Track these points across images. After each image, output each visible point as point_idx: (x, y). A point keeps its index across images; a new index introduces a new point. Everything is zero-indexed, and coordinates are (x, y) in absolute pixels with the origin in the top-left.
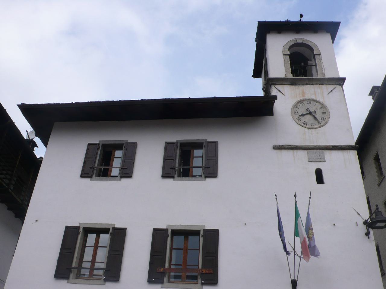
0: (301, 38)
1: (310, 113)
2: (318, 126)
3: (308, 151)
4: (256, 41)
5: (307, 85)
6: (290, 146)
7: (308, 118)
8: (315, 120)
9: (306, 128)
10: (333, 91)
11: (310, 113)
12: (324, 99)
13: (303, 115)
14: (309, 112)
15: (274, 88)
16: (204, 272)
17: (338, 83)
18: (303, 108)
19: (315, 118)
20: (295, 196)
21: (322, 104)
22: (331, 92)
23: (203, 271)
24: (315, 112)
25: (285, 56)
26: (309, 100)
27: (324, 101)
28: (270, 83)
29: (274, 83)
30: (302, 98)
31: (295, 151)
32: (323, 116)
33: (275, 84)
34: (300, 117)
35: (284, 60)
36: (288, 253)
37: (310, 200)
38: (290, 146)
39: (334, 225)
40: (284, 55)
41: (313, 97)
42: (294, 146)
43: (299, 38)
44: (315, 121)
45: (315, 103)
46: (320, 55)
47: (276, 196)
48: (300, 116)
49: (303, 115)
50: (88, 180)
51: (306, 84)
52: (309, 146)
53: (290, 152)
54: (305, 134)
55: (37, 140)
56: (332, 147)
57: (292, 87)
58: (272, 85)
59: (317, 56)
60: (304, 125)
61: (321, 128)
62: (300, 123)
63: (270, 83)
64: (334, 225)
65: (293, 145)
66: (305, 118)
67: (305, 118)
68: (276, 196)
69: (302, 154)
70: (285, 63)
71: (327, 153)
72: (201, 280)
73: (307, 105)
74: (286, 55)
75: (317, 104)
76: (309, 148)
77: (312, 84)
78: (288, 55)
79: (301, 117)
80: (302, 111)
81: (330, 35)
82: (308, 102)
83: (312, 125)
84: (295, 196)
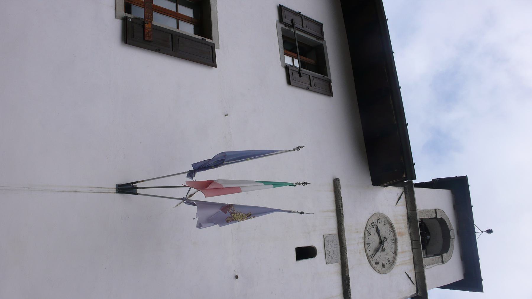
0: (454, 237)
1: (381, 243)
2: (369, 255)
3: (337, 236)
4: (433, 180)
5: (410, 241)
6: (342, 206)
7: (374, 240)
8: (375, 251)
9: (364, 234)
10: (409, 280)
11: (381, 243)
12: (399, 265)
13: (378, 231)
14: (382, 240)
15: (402, 191)
16: (146, 25)
17: (419, 289)
18: (386, 232)
19: (377, 250)
20: (304, 184)
21: (394, 263)
22: (407, 277)
23: (148, 23)
24: (383, 250)
25: (434, 211)
26: (395, 242)
27: (397, 265)
28: (406, 186)
29: (407, 192)
30: (397, 231)
31: (334, 214)
32: (380, 263)
33: (405, 192)
34: (375, 227)
35: (431, 210)
36: (191, 174)
37: (297, 212)
38: (341, 205)
39: (237, 277)
40: (435, 210)
41: (400, 249)
42: (342, 212)
43: (454, 233)
44: (374, 249)
45: (393, 251)
46: (443, 262)
47: (299, 148)
48: (377, 226)
49: (378, 231)
50: (219, 53)
51: (411, 239)
52: (345, 236)
53: (331, 205)
54: (357, 232)
55: (190, 180)
56: (347, 275)
57: (406, 218)
58: (404, 189)
59: (441, 258)
60: (367, 233)
61: (366, 257)
62: (368, 227)
63: (406, 186)
64: (237, 277)
65: (343, 209)
66: (375, 234)
67: (375, 234)
68: (299, 148)
69: (332, 227)
70: (428, 210)
71: (336, 268)
72: (132, 18)
73: (390, 237)
74: (436, 213)
75: (392, 255)
76: (342, 236)
77: (412, 249)
78: (436, 216)
79: (375, 229)
80: (384, 231)
81: (462, 279)
82: (392, 240)
83: (369, 244)
84: (304, 184)
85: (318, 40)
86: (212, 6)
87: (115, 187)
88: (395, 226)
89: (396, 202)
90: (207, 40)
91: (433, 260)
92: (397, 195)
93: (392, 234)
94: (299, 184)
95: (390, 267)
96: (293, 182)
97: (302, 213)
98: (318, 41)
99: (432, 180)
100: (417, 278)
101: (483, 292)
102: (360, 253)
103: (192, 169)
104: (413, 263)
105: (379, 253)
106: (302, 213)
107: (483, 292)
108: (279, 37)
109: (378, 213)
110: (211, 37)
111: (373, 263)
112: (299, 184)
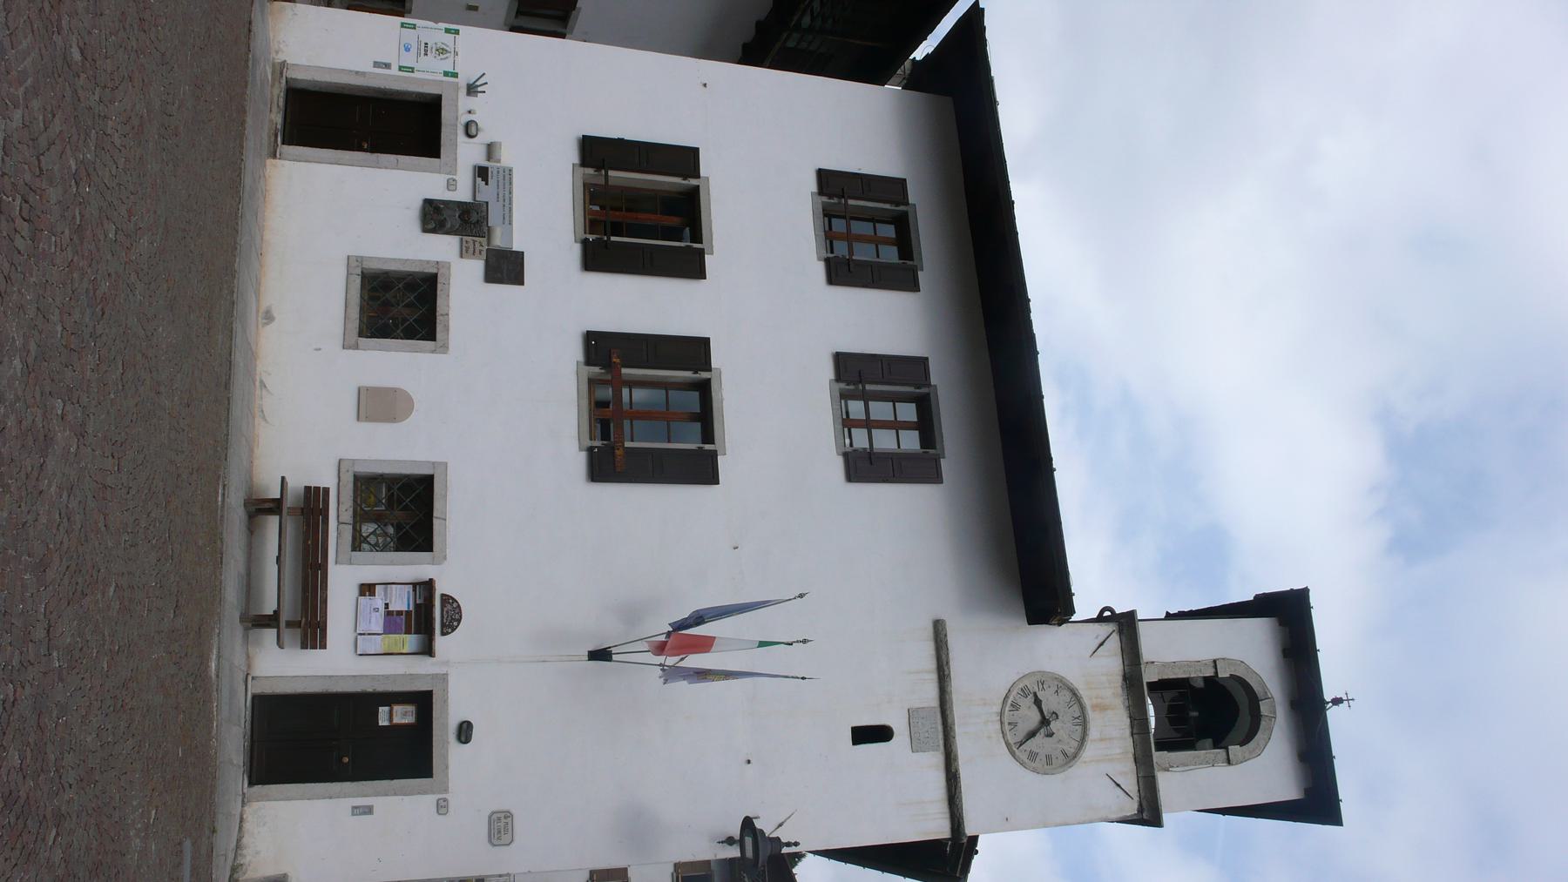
0: (1275, 713)
3: (939, 709)
4: (1257, 597)
6: (948, 663)
10: (1118, 788)
13: (1038, 702)
16: (616, 451)
19: (1032, 735)
20: (805, 641)
27: (1085, 762)
31: (934, 676)
39: (749, 762)
40: (1215, 661)
45: (1078, 736)
48: (1035, 694)
49: (1038, 702)
53: (931, 664)
62: (1014, 693)
64: (749, 762)
68: (801, 596)
71: (933, 761)
74: (1215, 667)
75: (1075, 744)
77: (1132, 734)
79: (1031, 698)
80: (1051, 702)
84: (805, 641)
85: (918, 388)
86: (713, 394)
87: (587, 653)
88: (1083, 693)
89: (1095, 649)
90: (909, 262)
91: (1199, 757)
92: (1097, 637)
93: (1076, 708)
94: (797, 642)
95: (1066, 764)
96: (790, 641)
97: (803, 678)
98: (918, 391)
99: (1255, 597)
100: (1141, 786)
101: (1342, 825)
102: (989, 737)
103: (671, 629)
104: (1133, 759)
105: (1039, 738)
106: (803, 678)
107: (1342, 825)
108: (835, 407)
109: (1040, 672)
110: (911, 259)
111: (1024, 757)
112: (797, 642)
